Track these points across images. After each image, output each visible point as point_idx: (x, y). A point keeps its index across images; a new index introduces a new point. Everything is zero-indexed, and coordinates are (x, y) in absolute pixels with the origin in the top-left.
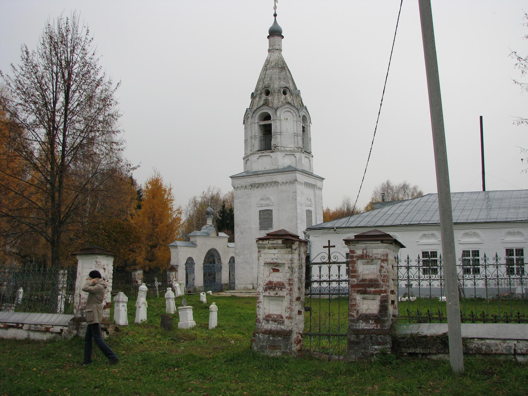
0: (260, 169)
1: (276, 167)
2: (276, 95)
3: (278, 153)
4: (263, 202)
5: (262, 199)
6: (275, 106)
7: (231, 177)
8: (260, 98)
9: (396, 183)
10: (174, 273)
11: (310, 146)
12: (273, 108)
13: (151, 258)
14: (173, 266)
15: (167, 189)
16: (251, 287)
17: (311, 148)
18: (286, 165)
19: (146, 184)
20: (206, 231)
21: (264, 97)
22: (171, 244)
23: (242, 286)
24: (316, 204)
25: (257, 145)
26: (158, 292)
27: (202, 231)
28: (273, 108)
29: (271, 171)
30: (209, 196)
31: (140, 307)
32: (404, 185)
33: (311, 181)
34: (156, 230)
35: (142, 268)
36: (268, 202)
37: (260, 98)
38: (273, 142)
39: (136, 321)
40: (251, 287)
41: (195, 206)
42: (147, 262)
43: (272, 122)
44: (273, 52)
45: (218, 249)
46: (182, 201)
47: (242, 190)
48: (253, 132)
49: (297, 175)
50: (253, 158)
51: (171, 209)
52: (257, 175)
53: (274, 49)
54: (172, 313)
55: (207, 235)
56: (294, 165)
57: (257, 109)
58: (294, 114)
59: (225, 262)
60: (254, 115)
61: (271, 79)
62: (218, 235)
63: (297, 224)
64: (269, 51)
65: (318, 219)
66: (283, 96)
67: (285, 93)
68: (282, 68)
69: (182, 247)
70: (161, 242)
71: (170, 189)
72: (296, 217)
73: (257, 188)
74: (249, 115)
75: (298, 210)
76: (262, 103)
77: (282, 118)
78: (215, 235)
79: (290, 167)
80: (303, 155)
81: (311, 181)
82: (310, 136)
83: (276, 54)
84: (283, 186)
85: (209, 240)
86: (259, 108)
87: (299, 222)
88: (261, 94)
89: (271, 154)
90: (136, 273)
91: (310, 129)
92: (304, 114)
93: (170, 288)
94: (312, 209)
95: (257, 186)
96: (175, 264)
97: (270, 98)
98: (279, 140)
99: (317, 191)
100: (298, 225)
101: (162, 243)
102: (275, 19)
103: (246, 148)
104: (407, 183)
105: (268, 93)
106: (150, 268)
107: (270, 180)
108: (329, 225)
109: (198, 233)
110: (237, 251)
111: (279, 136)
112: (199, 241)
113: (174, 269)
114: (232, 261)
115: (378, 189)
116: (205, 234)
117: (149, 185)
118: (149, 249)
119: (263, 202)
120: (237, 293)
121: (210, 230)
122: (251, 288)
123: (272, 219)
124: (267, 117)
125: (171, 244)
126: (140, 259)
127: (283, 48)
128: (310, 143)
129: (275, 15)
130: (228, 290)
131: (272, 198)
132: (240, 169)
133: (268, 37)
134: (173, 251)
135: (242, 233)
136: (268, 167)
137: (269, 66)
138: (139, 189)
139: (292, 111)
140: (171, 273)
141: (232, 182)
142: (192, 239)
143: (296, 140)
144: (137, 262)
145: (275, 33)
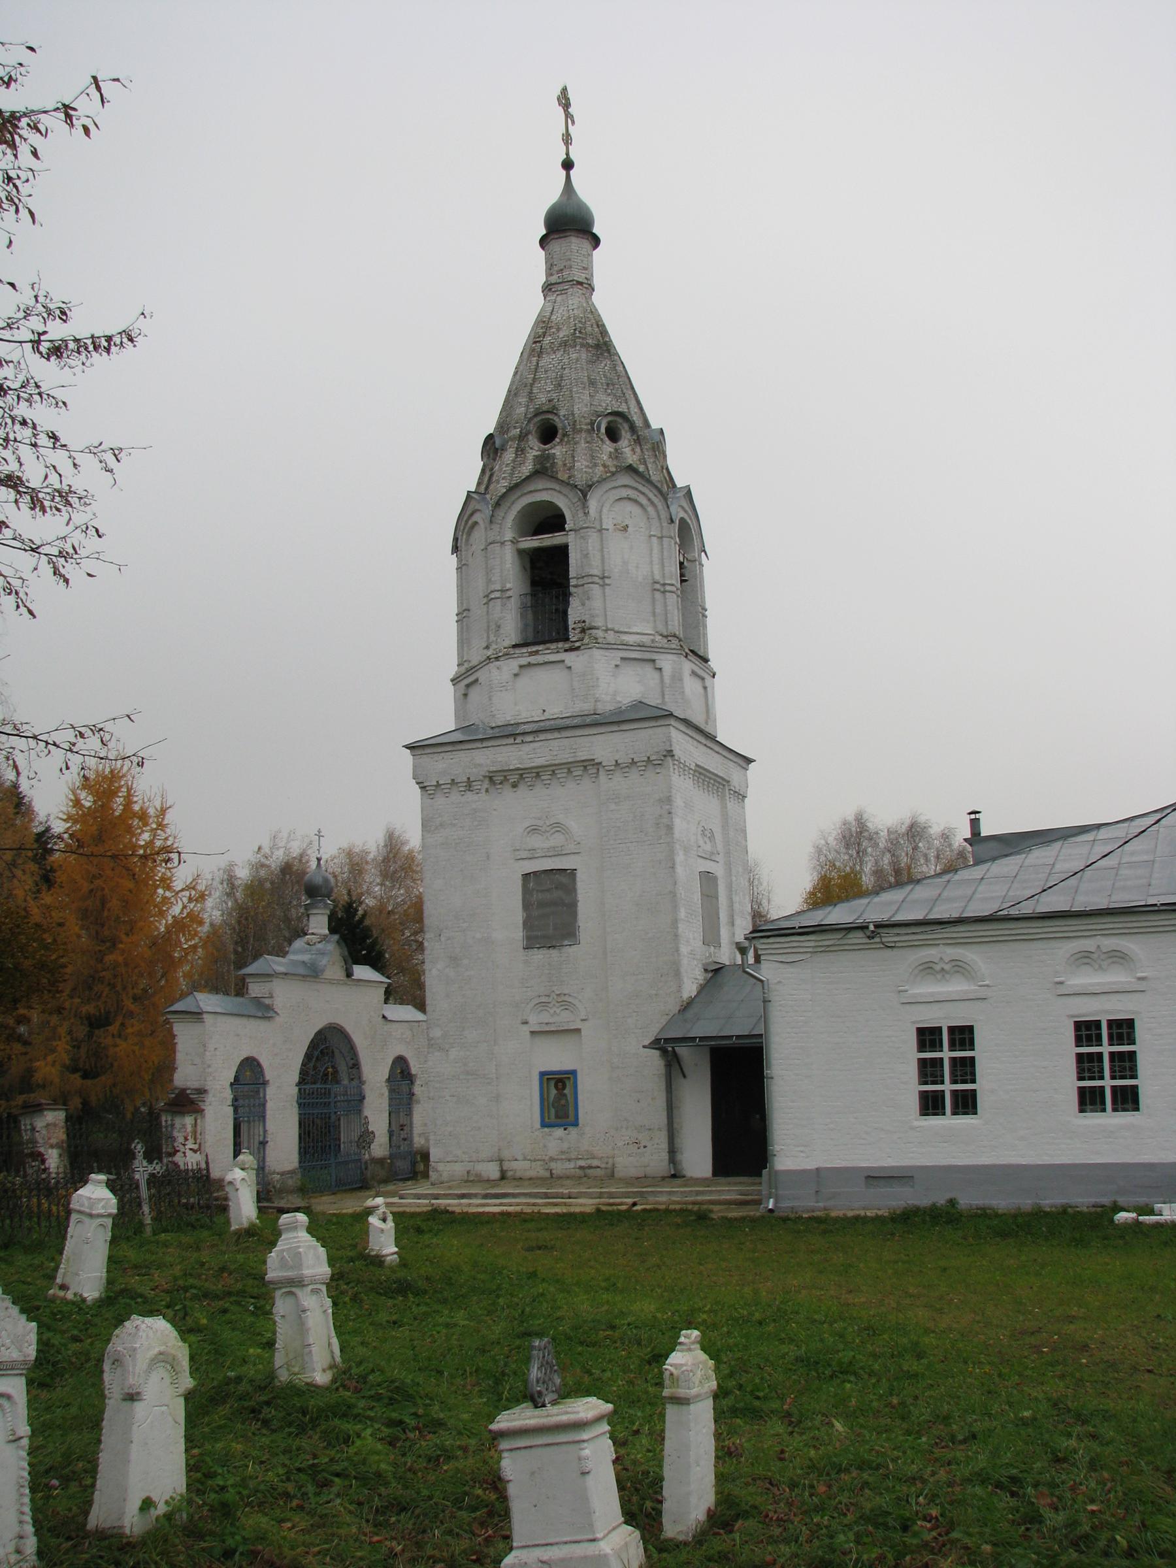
0: (524, 716)
1: (587, 707)
2: (582, 438)
3: (597, 653)
4: (537, 842)
5: (534, 830)
6: (580, 479)
7: (410, 747)
8: (520, 451)
9: (886, 817)
10: (189, 1120)
11: (705, 635)
12: (565, 499)
13: (89, 1066)
14: (183, 1091)
15: (151, 811)
16: (493, 1171)
17: (706, 643)
18: (625, 700)
19: (74, 793)
20: (306, 957)
21: (534, 448)
22: (178, 1007)
23: (459, 1169)
24: (728, 853)
25: (510, 622)
26: (146, 1209)
27: (291, 957)
28: (565, 499)
29: (568, 722)
30: (278, 858)
31: (132, 1397)
32: (912, 826)
33: (714, 763)
34: (110, 958)
35: (61, 1100)
36: (557, 840)
37: (520, 451)
38: (575, 613)
39: (98, 1517)
40: (493, 1171)
41: (230, 894)
42: (76, 1079)
43: (571, 540)
44: (563, 292)
45: (349, 1029)
46: (211, 843)
47: (455, 796)
48: (496, 577)
49: (674, 734)
50: (495, 672)
51: (166, 883)
52: (514, 736)
53: (566, 282)
54: (321, 1378)
55: (313, 973)
56: (654, 700)
57: (512, 489)
58: (650, 509)
59: (375, 1076)
60: (500, 513)
61: (559, 386)
62: (349, 975)
63: (675, 923)
64: (548, 288)
65: (736, 906)
66: (608, 447)
67: (613, 434)
68: (597, 346)
69: (221, 1018)
70: (129, 1004)
71: (163, 811)
72: (673, 894)
73: (514, 786)
74: (477, 517)
75: (679, 870)
76: (527, 468)
77: (608, 523)
78: (340, 974)
79: (640, 704)
80: (687, 666)
81: (714, 763)
82: (703, 598)
83: (574, 299)
84: (618, 777)
85: (311, 995)
86: (517, 486)
87: (682, 914)
88: (522, 437)
89: (570, 658)
90: (40, 1123)
91: (701, 572)
92: (682, 514)
93: (302, 1217)
94: (718, 870)
95: (513, 778)
96: (193, 1083)
97: (558, 450)
98: (596, 604)
99: (731, 805)
100: (681, 927)
101: (132, 1007)
102: (568, 177)
103: (463, 642)
104: (922, 819)
105: (548, 434)
106: (85, 1103)
107: (565, 757)
108: (838, 915)
109: (277, 964)
110: (437, 1033)
111: (596, 590)
112: (283, 995)
113: (187, 1103)
114: (401, 1073)
115: (831, 840)
116: (302, 971)
117: (83, 795)
118: (81, 1031)
119: (537, 842)
120: (446, 1196)
121: (322, 953)
122: (496, 1175)
123: (572, 907)
124: (552, 521)
125: (178, 1007)
126: (47, 1069)
127: (596, 282)
128: (705, 626)
129: (568, 165)
130: (386, 1181)
131: (573, 825)
132: (439, 716)
133: (543, 242)
134: (184, 1034)
135: (454, 960)
136: (557, 709)
137: (548, 339)
138: (41, 829)
139: (644, 501)
140: (178, 1121)
141: (415, 767)
142: (255, 989)
143: (659, 609)
144: (38, 1077)
145: (568, 225)
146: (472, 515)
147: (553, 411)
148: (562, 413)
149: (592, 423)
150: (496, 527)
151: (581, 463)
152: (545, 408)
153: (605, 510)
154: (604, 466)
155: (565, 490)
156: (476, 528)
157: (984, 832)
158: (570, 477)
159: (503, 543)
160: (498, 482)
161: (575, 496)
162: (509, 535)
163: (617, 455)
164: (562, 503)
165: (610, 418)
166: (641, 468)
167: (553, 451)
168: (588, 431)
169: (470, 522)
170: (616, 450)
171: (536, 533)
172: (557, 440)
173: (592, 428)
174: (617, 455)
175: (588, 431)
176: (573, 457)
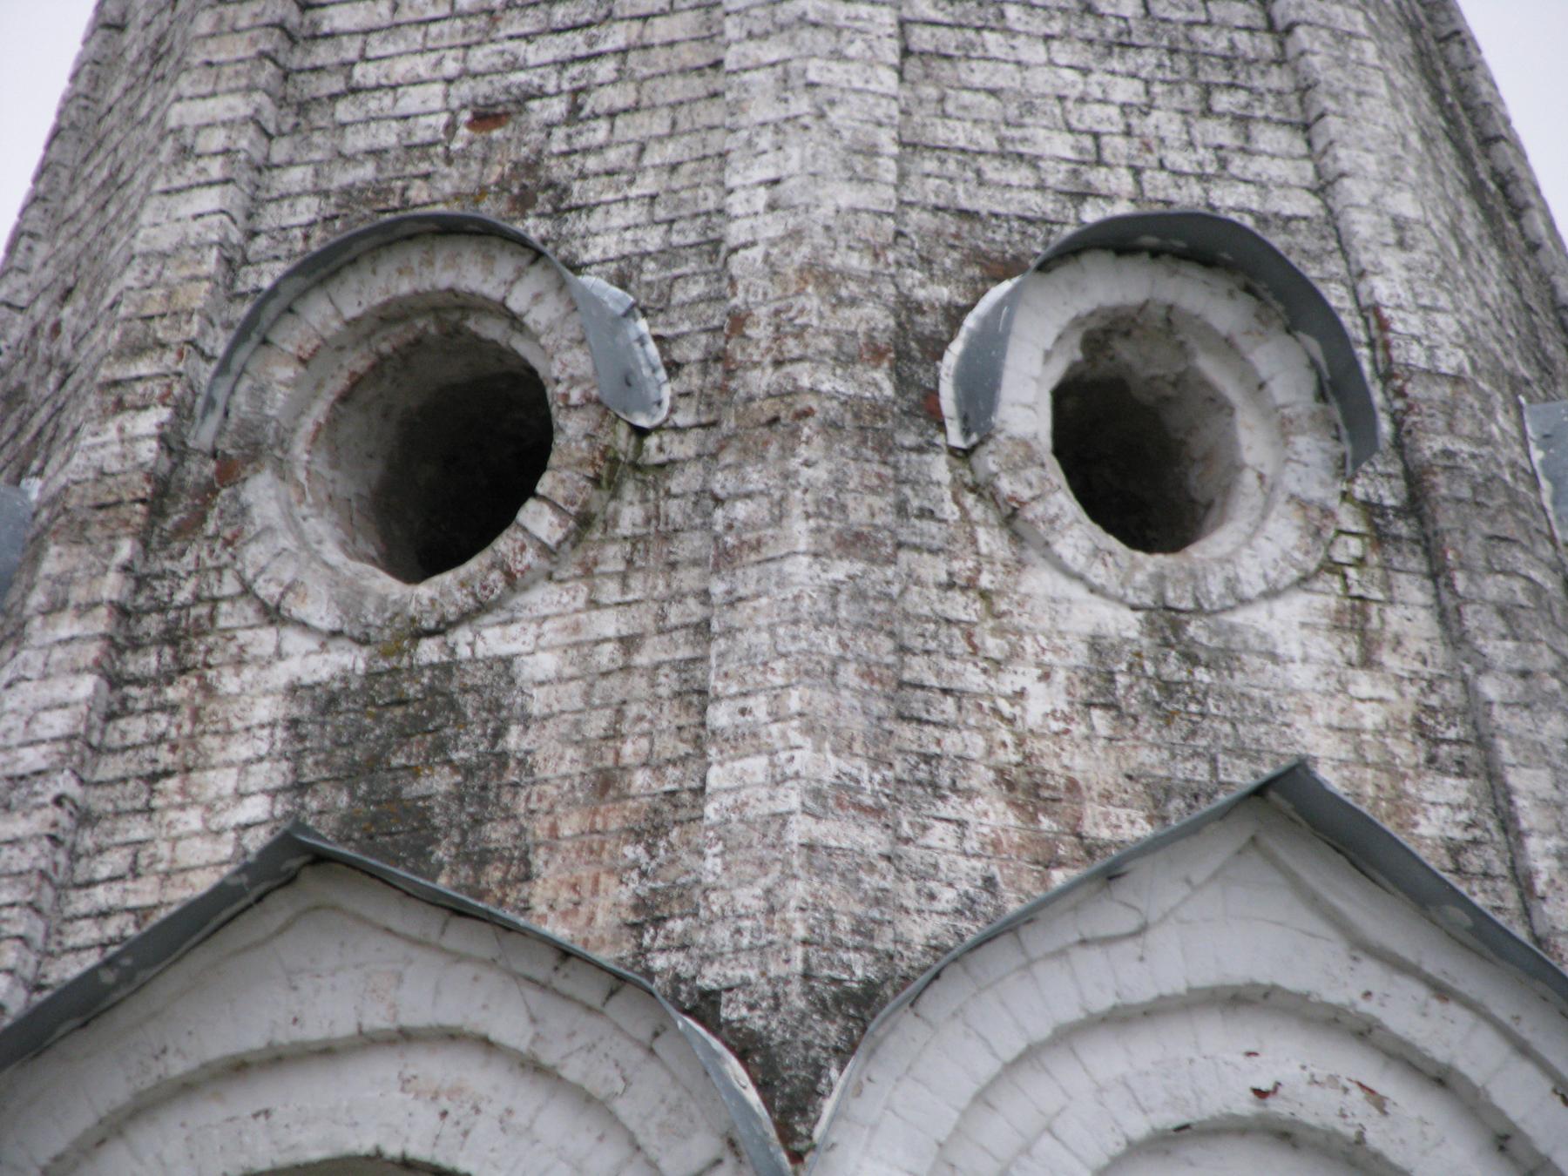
6: (754, 928)
8: (159, 645)
21: (304, 593)
66: (1080, 587)
67: (1134, 463)
88: (181, 500)
97: (540, 629)
105: (459, 460)
147: (512, 219)
148: (607, 234)
149: (911, 347)
151: (777, 765)
152: (437, 192)
154: (1027, 789)
155: (592, 1049)
158: (647, 914)
163: (1171, 670)
165: (1110, 287)
166: (1436, 815)
167: (493, 640)
168: (867, 427)
170: (1166, 621)
172: (540, 519)
173: (916, 384)
174: (1171, 670)
175: (867, 427)
176: (697, 697)
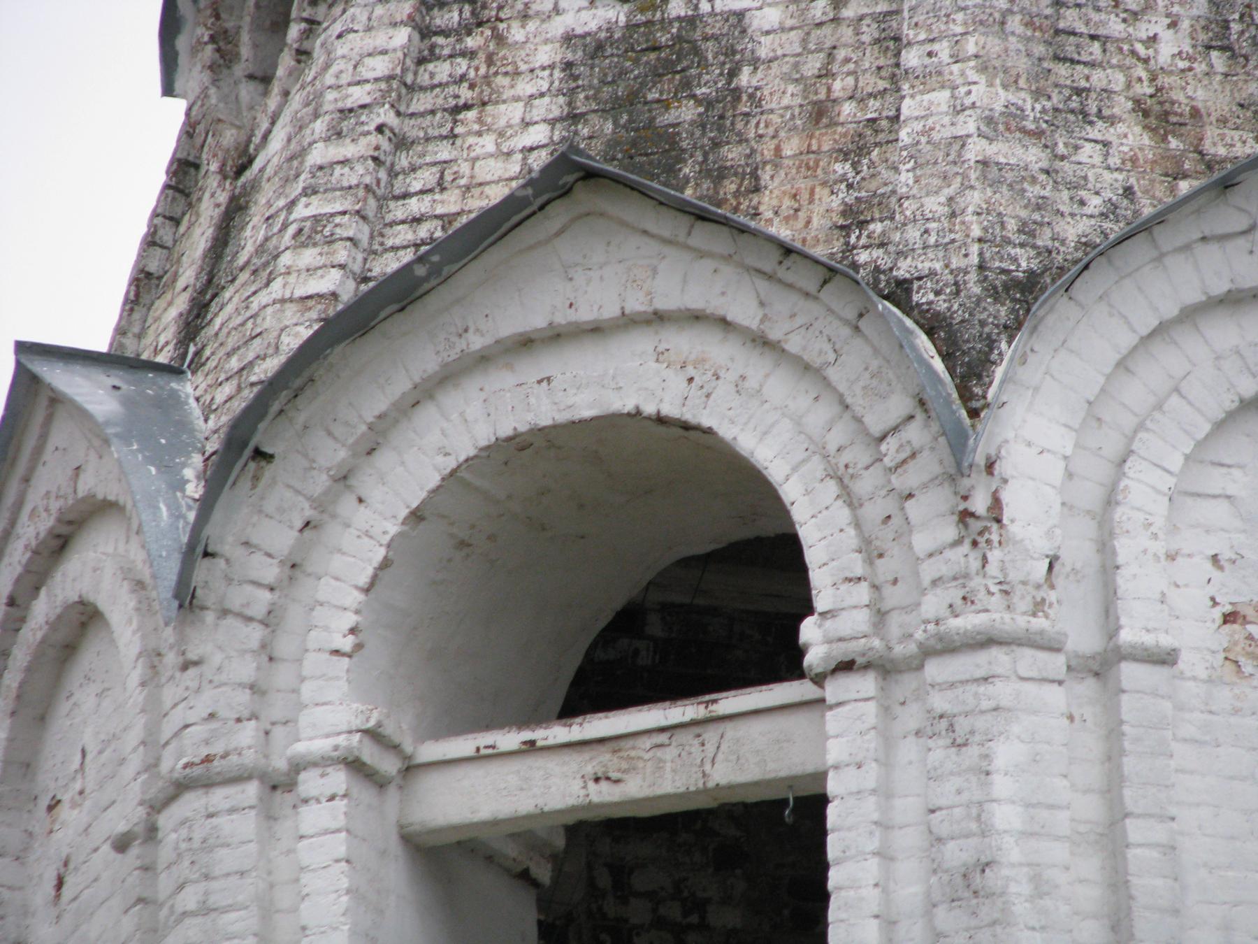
60: (264, 525)
124: (706, 599)
146: (60, 544)
150: (226, 647)
153: (1144, 491)
154: (1159, 116)
155: (809, 327)
156: (89, 658)
157: (1077, 426)
158: (853, 219)
159: (280, 785)
160: (265, 267)
161: (883, 373)
162: (330, 710)
164: (776, 431)
169: (42, 610)
171: (570, 710)
